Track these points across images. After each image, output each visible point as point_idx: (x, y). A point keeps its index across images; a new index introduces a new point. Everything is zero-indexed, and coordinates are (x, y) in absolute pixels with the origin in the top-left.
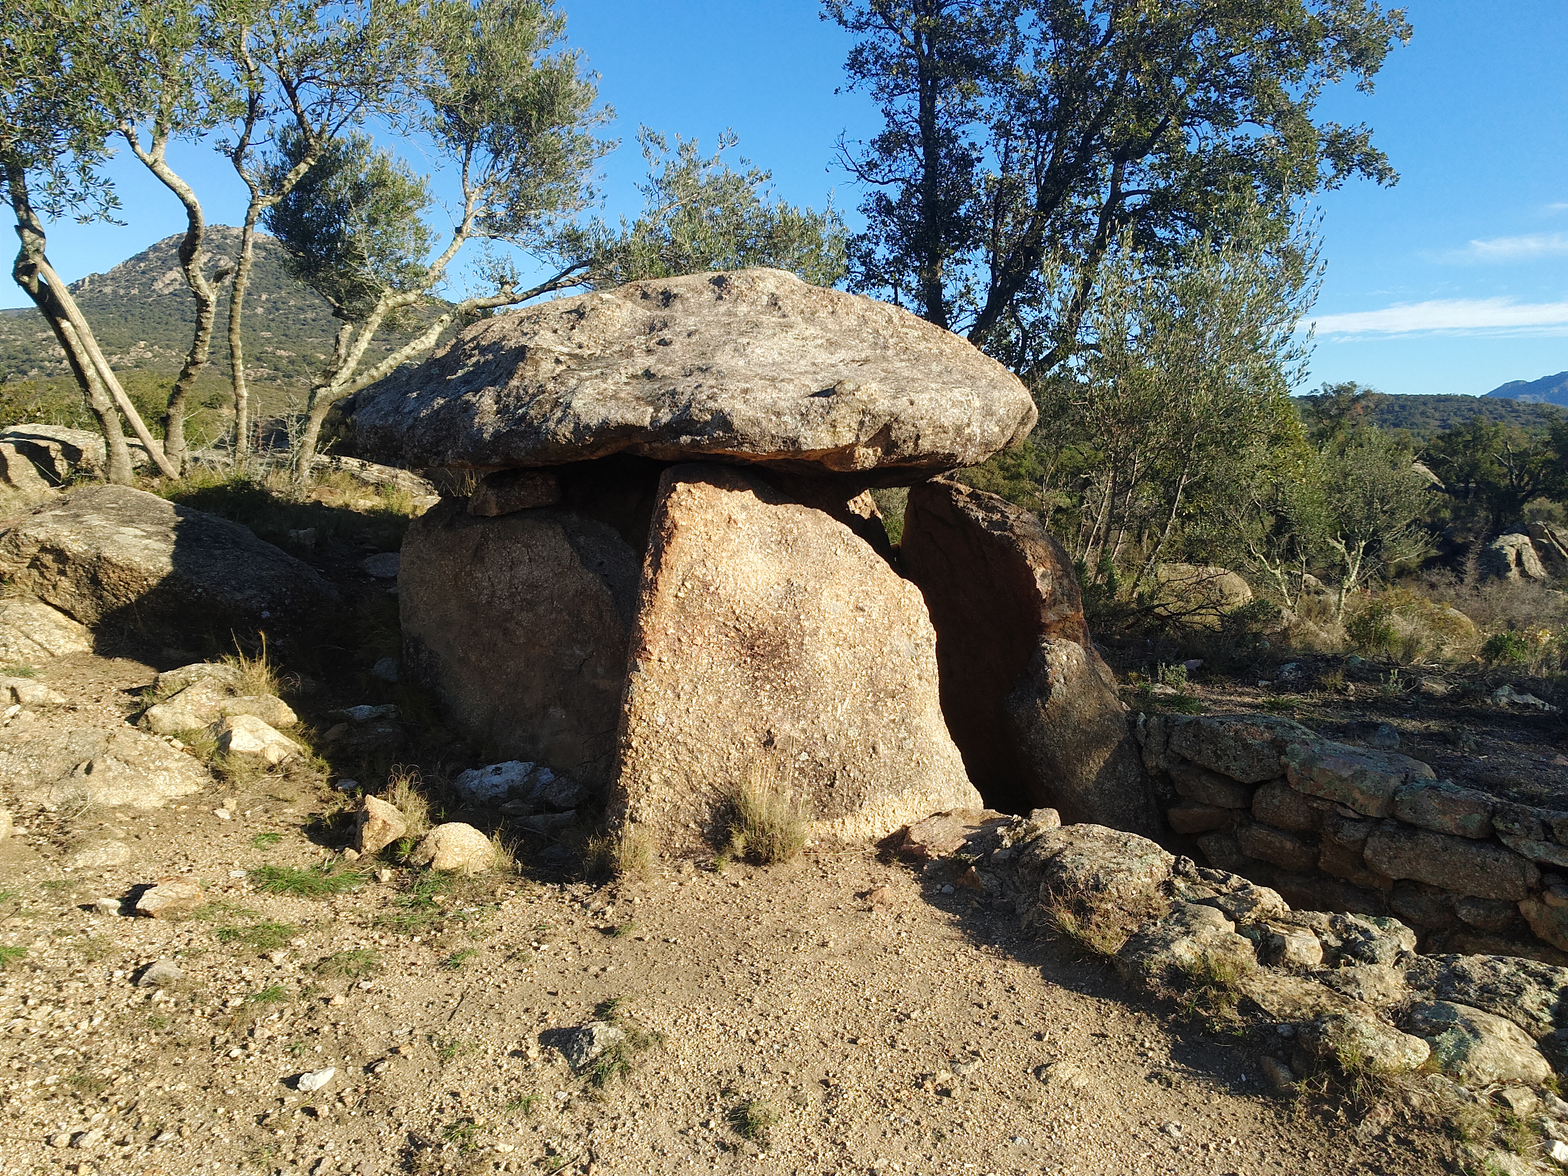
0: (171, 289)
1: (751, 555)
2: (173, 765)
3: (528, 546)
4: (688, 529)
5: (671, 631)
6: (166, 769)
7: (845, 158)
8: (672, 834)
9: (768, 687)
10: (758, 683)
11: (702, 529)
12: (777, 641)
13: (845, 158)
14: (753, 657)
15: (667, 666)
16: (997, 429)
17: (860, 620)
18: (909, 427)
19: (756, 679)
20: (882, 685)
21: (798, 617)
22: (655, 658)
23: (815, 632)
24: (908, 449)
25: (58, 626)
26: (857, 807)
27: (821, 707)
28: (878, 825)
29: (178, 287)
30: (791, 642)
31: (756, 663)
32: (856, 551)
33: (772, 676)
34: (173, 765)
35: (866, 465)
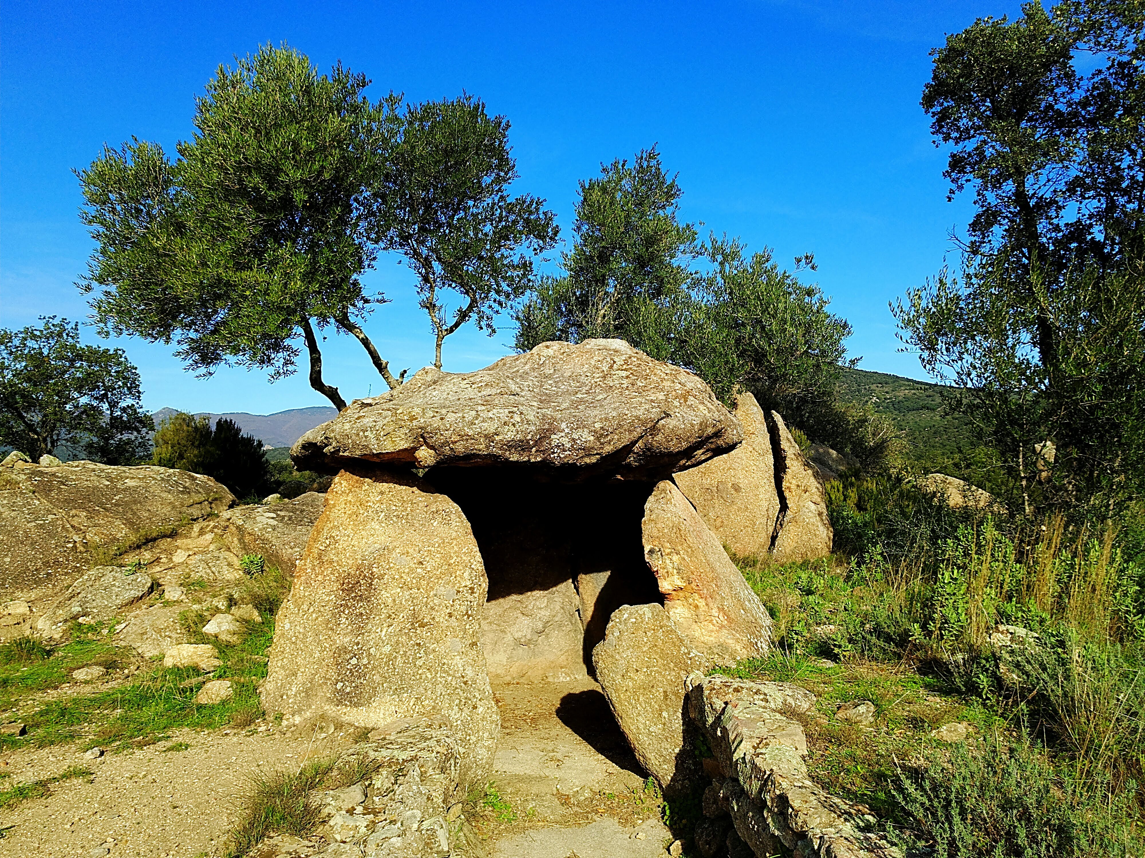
1: (375, 525)
17: (419, 570)
23: (381, 577)
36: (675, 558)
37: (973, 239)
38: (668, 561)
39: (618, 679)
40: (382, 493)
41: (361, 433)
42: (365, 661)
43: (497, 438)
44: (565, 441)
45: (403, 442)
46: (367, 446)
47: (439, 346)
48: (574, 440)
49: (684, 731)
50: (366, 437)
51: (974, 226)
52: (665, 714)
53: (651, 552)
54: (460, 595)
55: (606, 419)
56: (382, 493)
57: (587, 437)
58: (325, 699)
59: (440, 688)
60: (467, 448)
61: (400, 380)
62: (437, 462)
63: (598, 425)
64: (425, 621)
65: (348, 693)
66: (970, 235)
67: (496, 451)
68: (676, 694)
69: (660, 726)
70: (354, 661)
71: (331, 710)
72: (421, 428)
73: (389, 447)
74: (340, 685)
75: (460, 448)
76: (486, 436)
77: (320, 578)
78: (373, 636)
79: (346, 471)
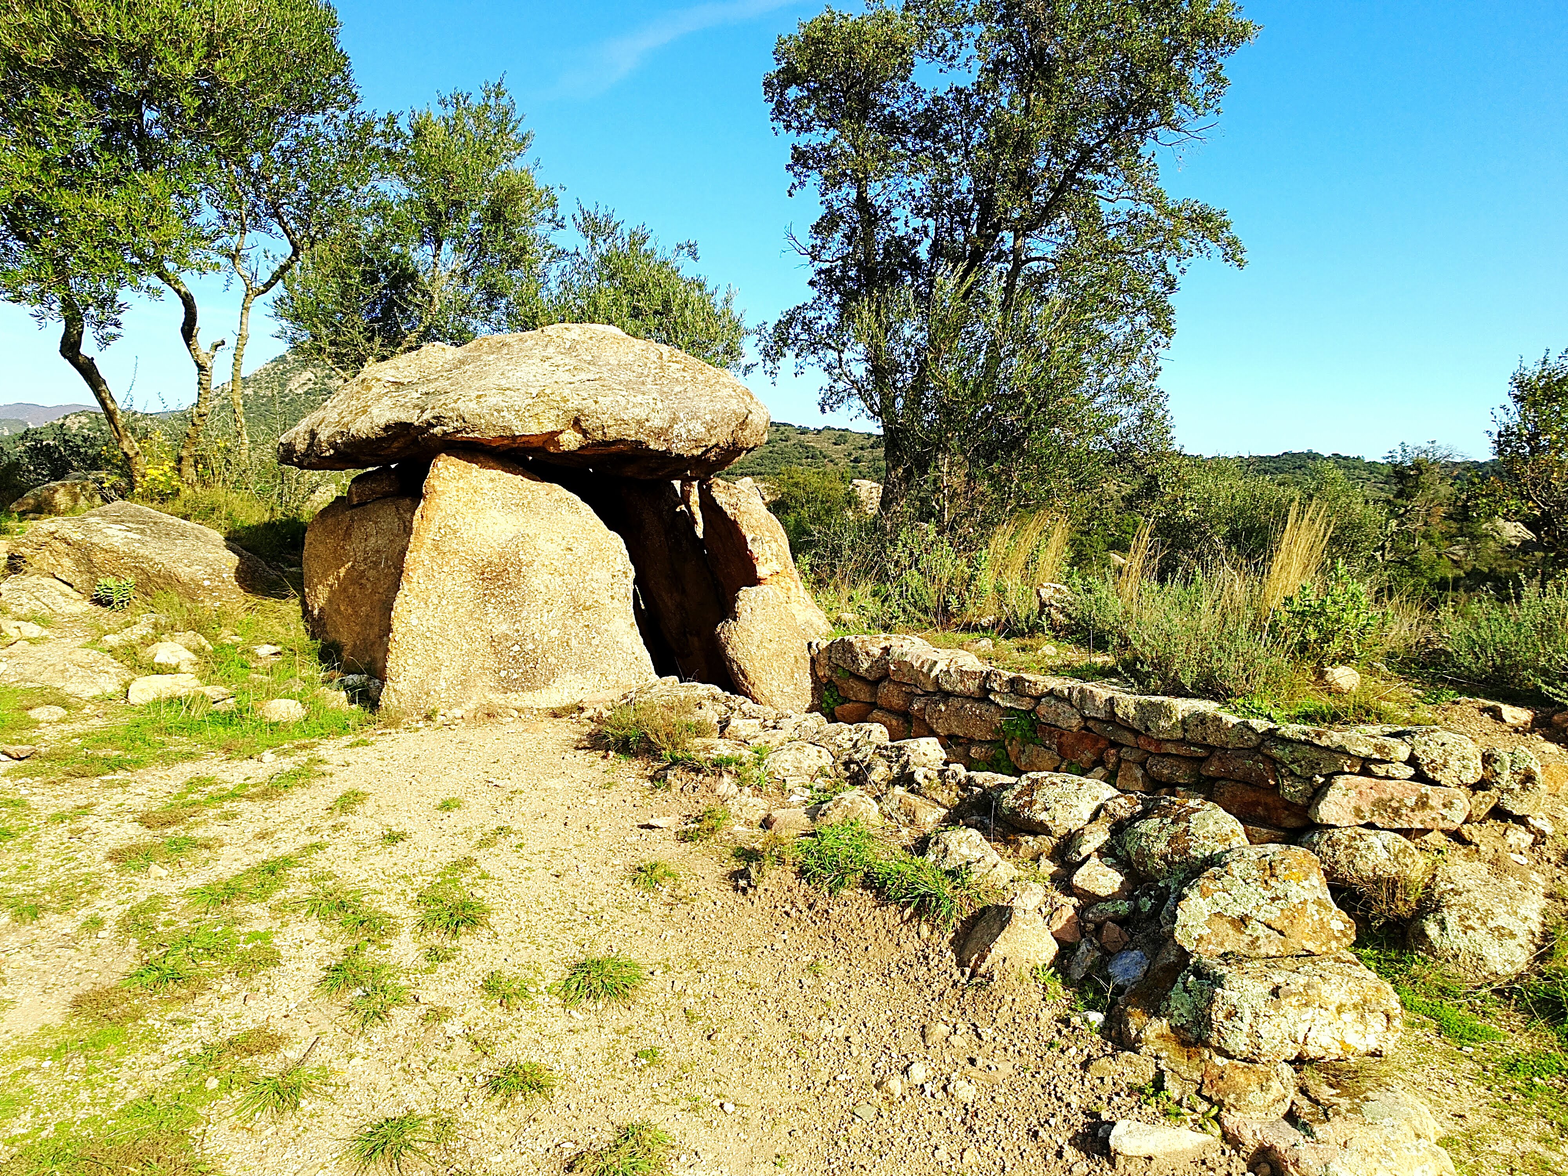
0: (306, 388)
1: (494, 513)
2: (112, 670)
3: (376, 523)
4: (444, 493)
5: (426, 563)
6: (107, 672)
7: (797, 247)
8: (419, 698)
9: (493, 601)
10: (486, 598)
11: (455, 493)
12: (501, 569)
13: (797, 247)
14: (483, 580)
15: (423, 587)
16: (703, 430)
17: (569, 557)
18: (594, 419)
19: (485, 595)
20: (581, 602)
21: (517, 553)
22: (415, 580)
23: (530, 564)
24: (599, 436)
25: (62, 594)
26: (551, 682)
27: (532, 615)
28: (566, 694)
29: (312, 386)
30: (510, 569)
31: (485, 584)
32: (578, 512)
33: (496, 593)
34: (112, 670)
35: (571, 448)
36: (774, 545)
37: (814, 242)
38: (767, 548)
39: (753, 649)
40: (492, 480)
41: (496, 414)
42: (531, 646)
43: (647, 424)
44: (683, 431)
45: (551, 424)
46: (504, 428)
47: (245, 309)
48: (689, 431)
49: (813, 689)
50: (503, 417)
51: (817, 229)
52: (796, 675)
53: (753, 540)
54: (616, 579)
55: (714, 412)
56: (492, 480)
57: (699, 429)
58: (487, 689)
59: (620, 664)
60: (619, 433)
61: (212, 353)
62: (582, 448)
63: (708, 417)
64: (588, 604)
65: (516, 679)
66: (811, 237)
67: (642, 437)
68: (804, 658)
69: (793, 687)
70: (517, 648)
71: (497, 698)
72: (578, 410)
73: (533, 429)
74: (503, 674)
75: (612, 434)
76: (638, 422)
77: (446, 569)
78: (533, 621)
79: (448, 455)
